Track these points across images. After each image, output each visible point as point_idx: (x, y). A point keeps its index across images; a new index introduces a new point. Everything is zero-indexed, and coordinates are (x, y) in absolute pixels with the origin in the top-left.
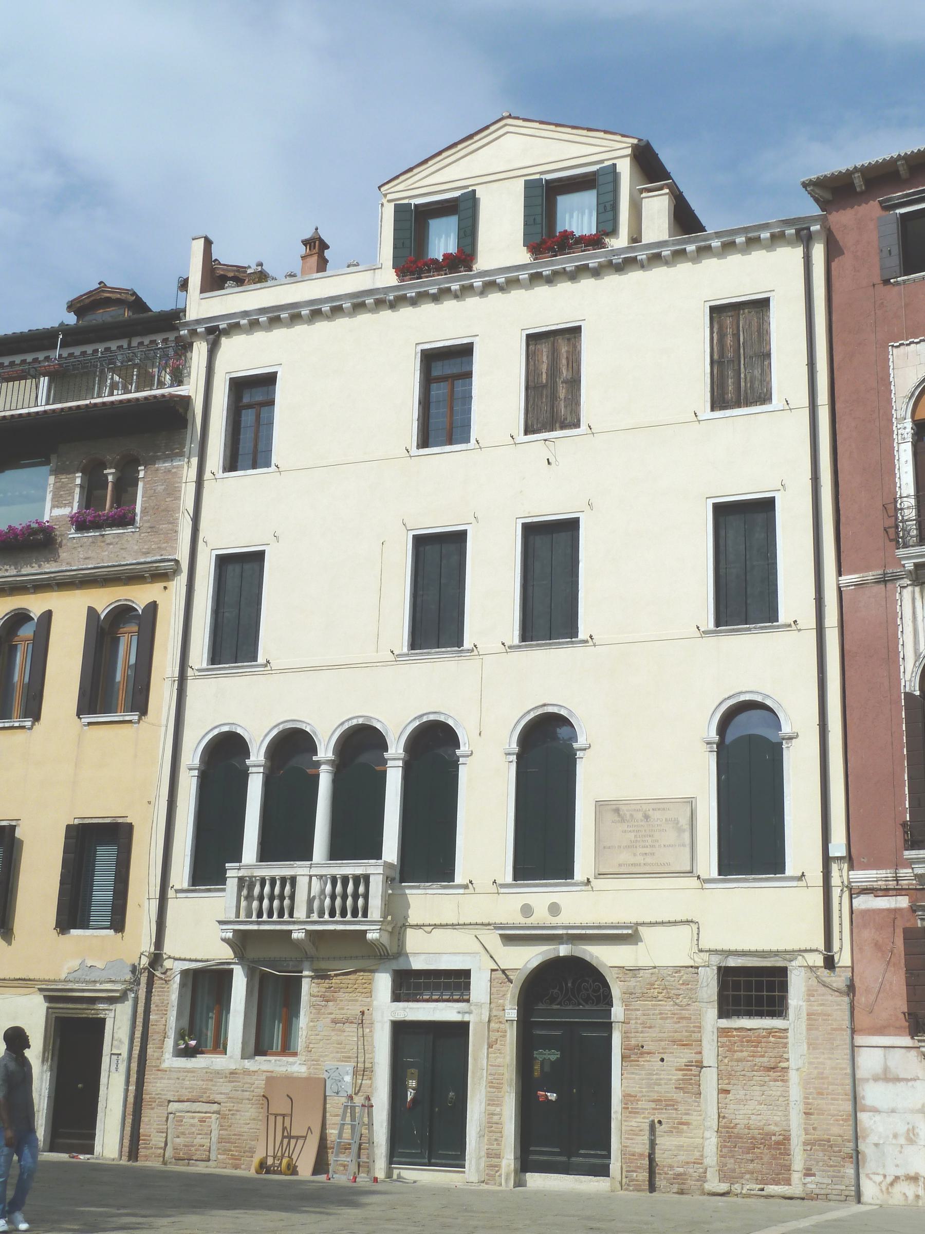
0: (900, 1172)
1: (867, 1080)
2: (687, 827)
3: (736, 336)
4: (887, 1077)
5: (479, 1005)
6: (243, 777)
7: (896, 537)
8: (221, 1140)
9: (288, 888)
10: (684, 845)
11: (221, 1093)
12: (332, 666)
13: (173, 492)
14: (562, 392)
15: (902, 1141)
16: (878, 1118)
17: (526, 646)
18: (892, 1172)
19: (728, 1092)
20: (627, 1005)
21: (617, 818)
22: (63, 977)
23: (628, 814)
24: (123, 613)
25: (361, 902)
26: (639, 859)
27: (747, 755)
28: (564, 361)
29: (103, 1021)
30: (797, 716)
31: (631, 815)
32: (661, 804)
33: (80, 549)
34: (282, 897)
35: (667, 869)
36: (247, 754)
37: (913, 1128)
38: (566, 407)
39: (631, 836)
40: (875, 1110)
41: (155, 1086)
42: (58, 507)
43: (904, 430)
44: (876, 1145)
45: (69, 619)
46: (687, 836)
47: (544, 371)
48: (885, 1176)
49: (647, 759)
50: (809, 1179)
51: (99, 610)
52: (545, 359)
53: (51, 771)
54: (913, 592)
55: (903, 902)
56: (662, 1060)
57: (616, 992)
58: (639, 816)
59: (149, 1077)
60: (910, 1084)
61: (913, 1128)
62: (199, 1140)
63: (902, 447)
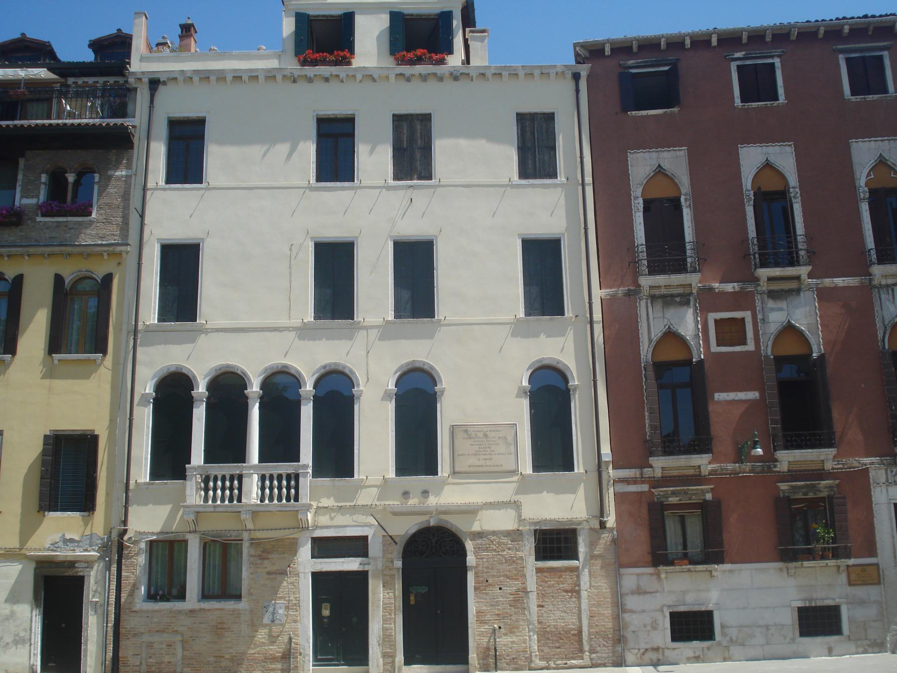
0: (648, 646)
4: (639, 591)
5: (375, 559)
6: (189, 403)
8: (184, 658)
12: (253, 325)
14: (418, 155)
15: (649, 628)
16: (634, 616)
17: (574, 523)
18: (643, 646)
19: (542, 606)
20: (476, 553)
21: (466, 436)
22: (47, 546)
25: (293, 491)
26: (482, 462)
27: (549, 396)
28: (419, 135)
34: (231, 489)
35: (499, 469)
39: (477, 448)
40: (632, 611)
41: (129, 623)
42: (26, 197)
43: (638, 205)
44: (634, 632)
46: (512, 448)
47: (405, 139)
49: (484, 397)
50: (594, 655)
53: (36, 396)
55: (645, 488)
56: (500, 589)
57: (469, 545)
58: (481, 435)
59: (123, 617)
62: (167, 659)
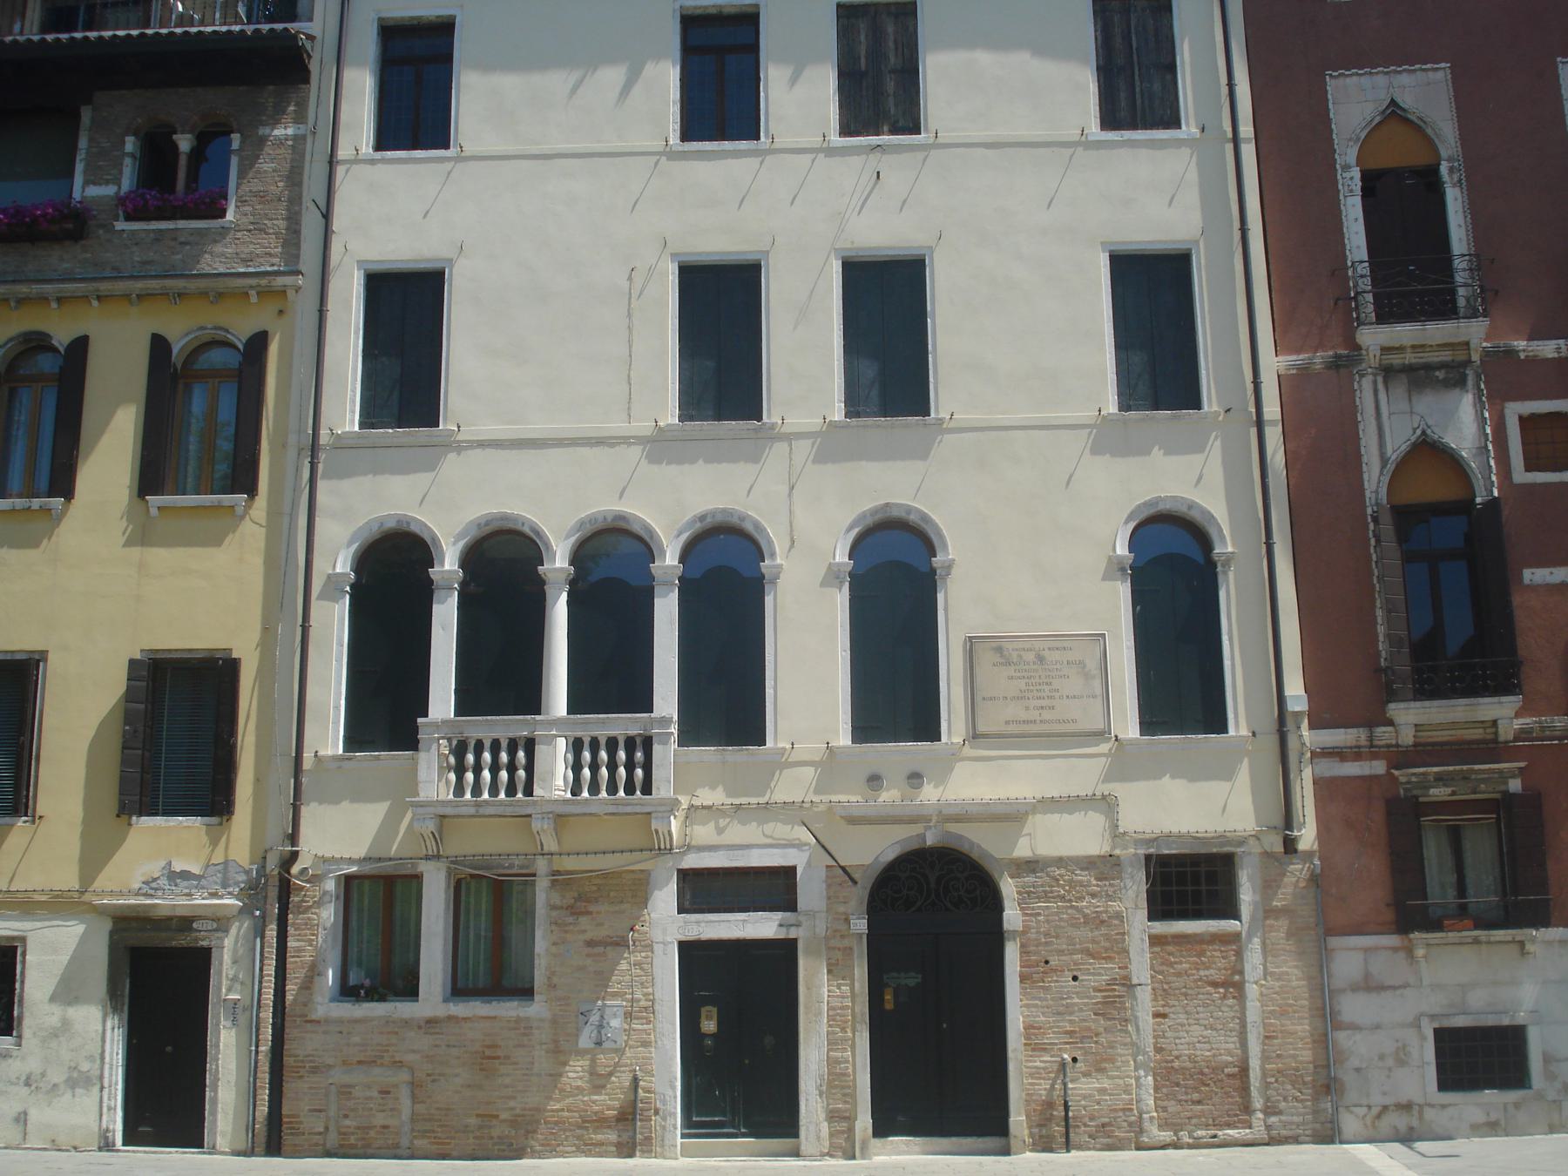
0: (1389, 1101)
1: (1343, 991)
2: (1096, 672)
3: (1127, 37)
4: (1369, 985)
5: (812, 914)
8: (414, 1118)
9: (521, 754)
10: (1094, 697)
11: (414, 1051)
12: (556, 433)
14: (890, 85)
15: (1390, 1062)
16: (1358, 1037)
18: (1378, 1100)
23: (1015, 654)
26: (1034, 715)
27: (1172, 576)
28: (891, 45)
29: (207, 952)
31: (1020, 656)
33: (135, 249)
37: (1404, 1046)
38: (896, 105)
39: (1022, 684)
40: (1354, 1027)
41: (301, 1045)
42: (94, 184)
43: (1350, 182)
44: (1358, 1070)
46: (1097, 685)
47: (863, 53)
48: (1369, 1107)
49: (1038, 576)
50: (1273, 1119)
51: (170, 337)
52: (862, 38)
54: (1375, 382)
56: (1075, 978)
58: (1030, 657)
59: (291, 1033)
60: (1398, 992)
61: (1404, 1046)
62: (380, 1120)
63: (1350, 201)
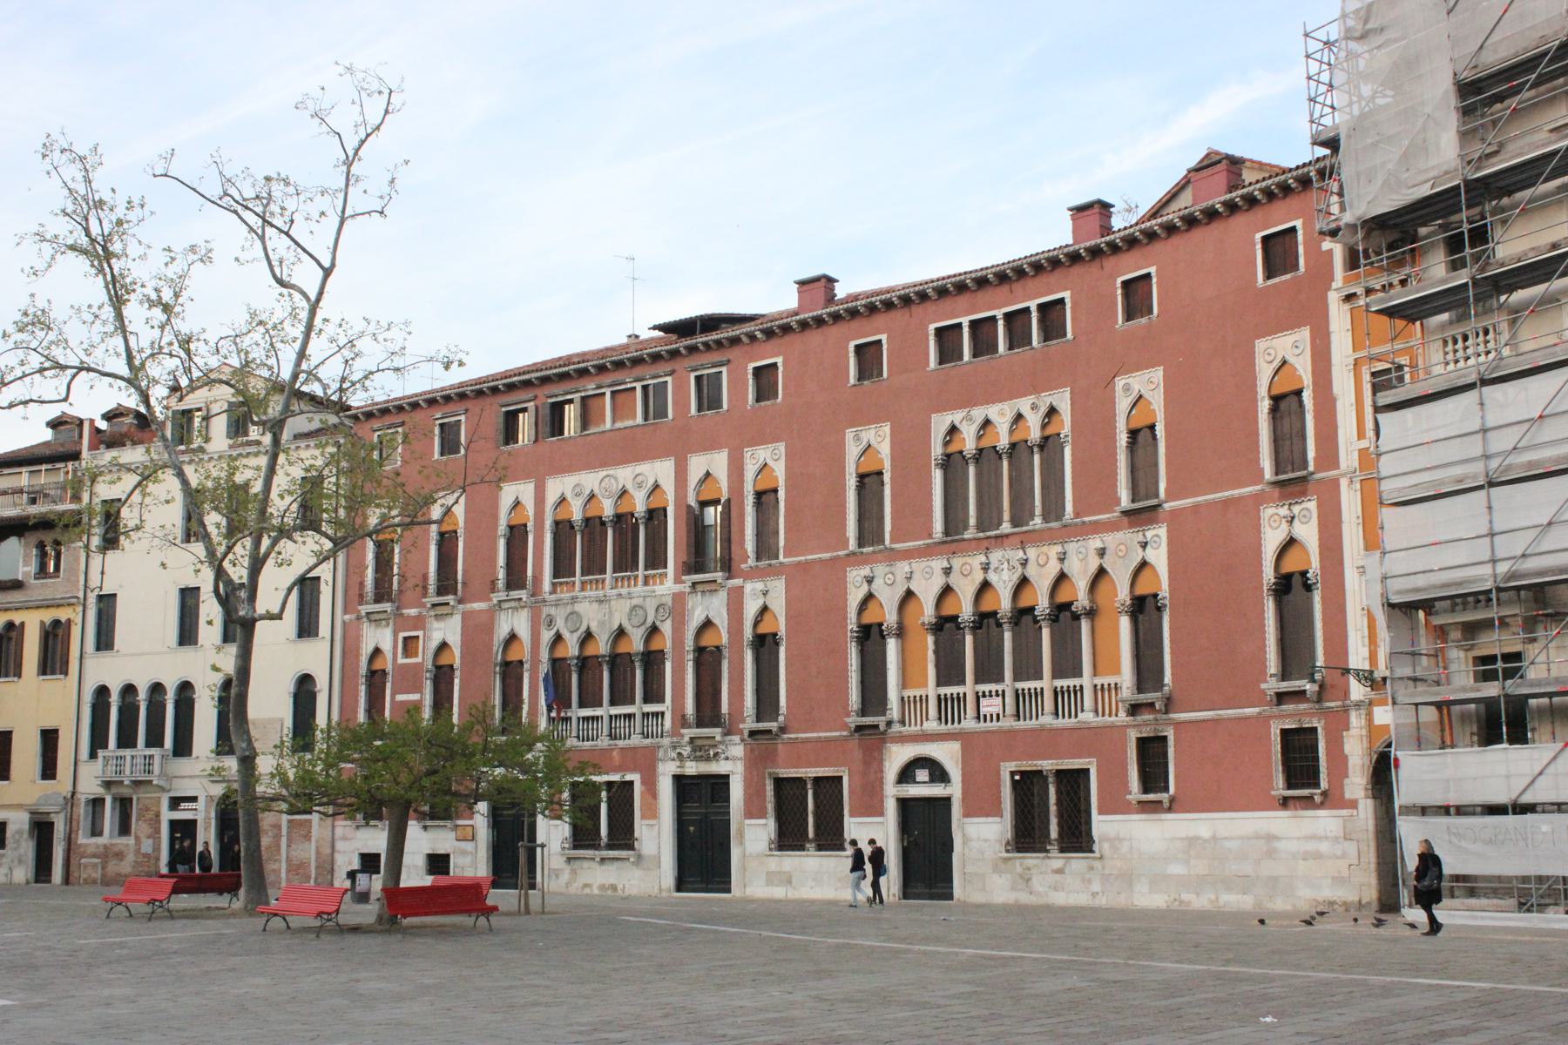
4: (345, 838)
7: (361, 598)
12: (145, 654)
13: (77, 559)
24: (57, 623)
30: (322, 683)
32: (271, 721)
36: (165, 693)
45: (33, 624)
